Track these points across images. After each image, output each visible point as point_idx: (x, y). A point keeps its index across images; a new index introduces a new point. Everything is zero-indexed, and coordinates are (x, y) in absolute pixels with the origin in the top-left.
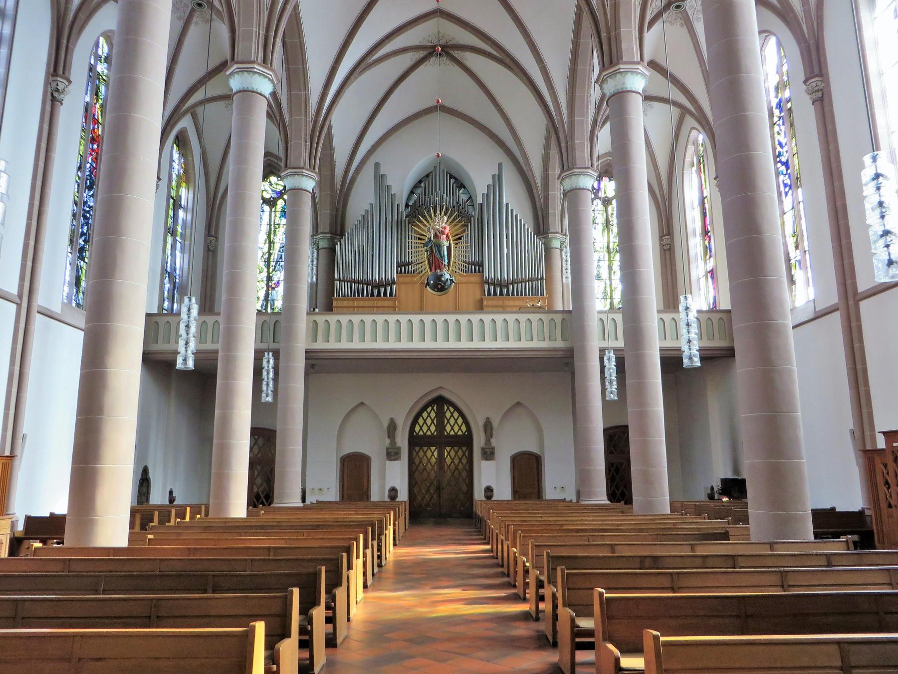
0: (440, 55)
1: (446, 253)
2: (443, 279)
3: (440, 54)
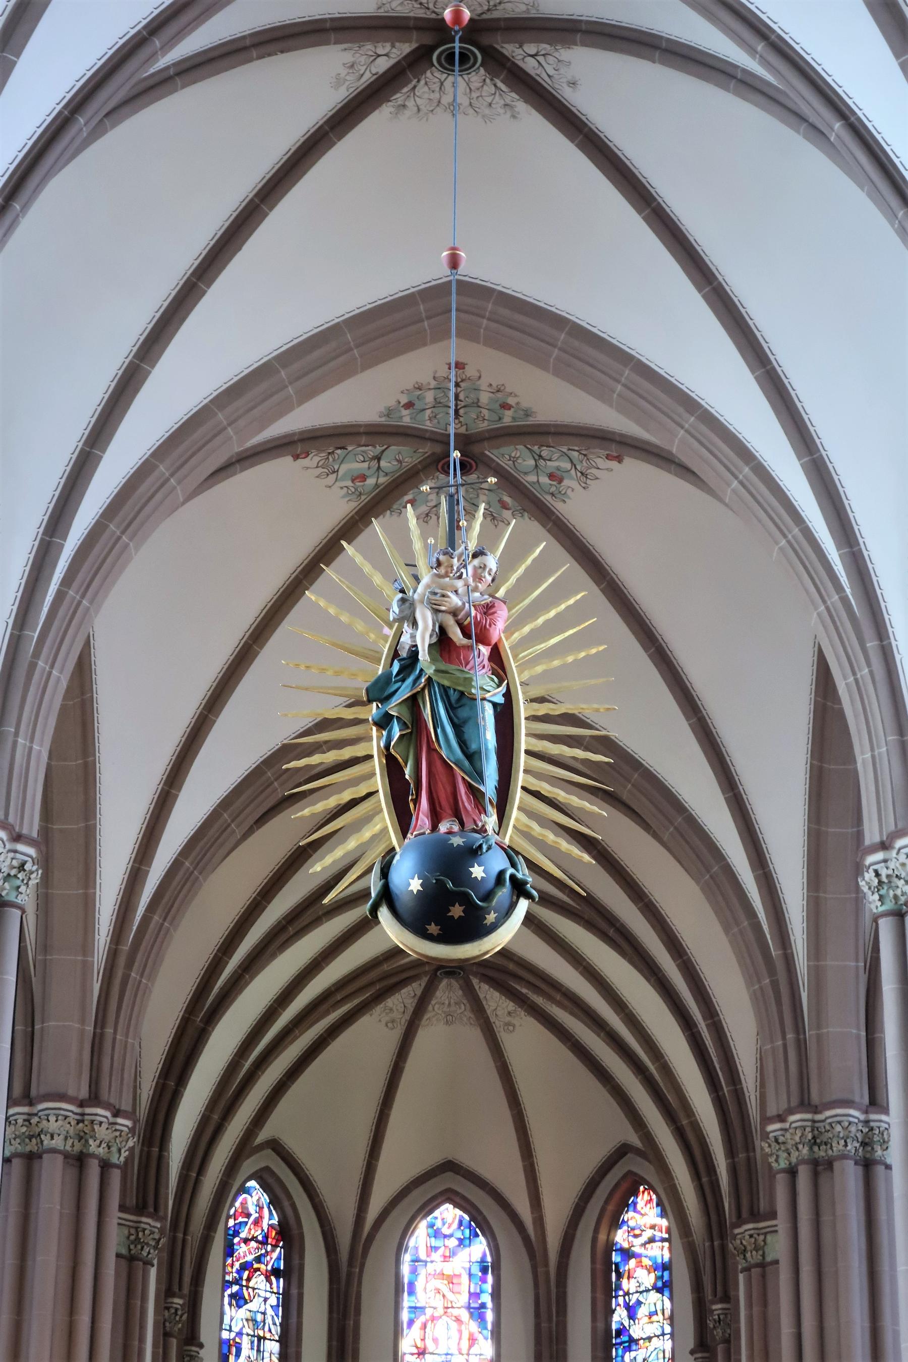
0: (464, 57)
1: (490, 737)
2: (477, 872)
3: (464, 57)
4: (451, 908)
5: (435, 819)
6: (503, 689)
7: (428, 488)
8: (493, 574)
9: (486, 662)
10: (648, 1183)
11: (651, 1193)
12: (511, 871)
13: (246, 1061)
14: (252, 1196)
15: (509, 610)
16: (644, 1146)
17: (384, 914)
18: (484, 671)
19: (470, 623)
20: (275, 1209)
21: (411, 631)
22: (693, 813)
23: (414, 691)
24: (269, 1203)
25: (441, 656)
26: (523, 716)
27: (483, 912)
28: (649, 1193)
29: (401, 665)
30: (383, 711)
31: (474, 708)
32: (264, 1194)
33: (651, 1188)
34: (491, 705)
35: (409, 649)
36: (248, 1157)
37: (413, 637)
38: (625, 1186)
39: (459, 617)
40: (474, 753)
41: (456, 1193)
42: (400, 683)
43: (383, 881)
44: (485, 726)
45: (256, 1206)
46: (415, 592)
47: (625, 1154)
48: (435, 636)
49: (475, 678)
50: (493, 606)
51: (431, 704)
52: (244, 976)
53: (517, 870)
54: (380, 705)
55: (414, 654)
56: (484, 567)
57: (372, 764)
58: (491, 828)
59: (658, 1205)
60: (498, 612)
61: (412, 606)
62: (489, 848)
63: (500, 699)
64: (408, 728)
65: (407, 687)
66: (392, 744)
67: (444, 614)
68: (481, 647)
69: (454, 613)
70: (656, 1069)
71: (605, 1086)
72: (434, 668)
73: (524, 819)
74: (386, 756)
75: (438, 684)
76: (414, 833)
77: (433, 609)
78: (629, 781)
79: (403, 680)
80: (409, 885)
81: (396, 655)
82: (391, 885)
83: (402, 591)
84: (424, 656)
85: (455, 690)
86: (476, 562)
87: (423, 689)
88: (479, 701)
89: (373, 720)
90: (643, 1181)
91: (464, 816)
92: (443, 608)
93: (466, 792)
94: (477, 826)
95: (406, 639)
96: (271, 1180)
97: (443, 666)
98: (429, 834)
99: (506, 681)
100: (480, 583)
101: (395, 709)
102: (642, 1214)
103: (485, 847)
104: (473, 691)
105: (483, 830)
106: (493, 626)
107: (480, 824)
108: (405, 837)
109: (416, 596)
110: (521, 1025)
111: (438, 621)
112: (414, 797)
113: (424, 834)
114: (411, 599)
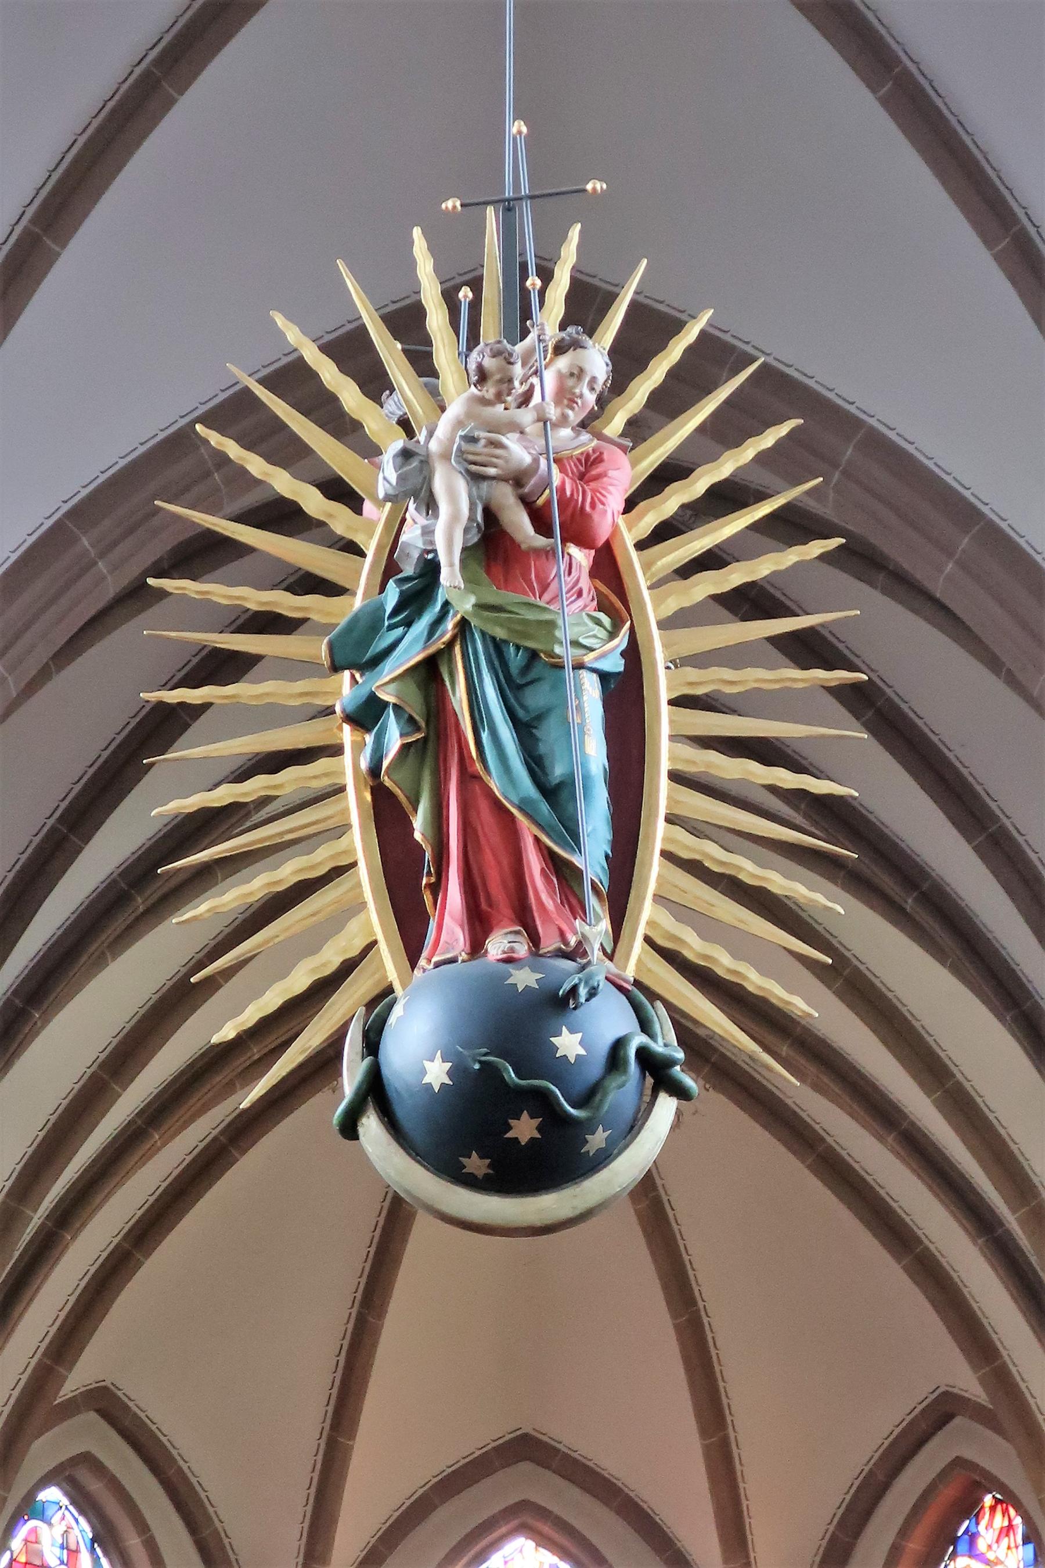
4: (513, 1122)
5: (478, 928)
6: (622, 641)
7: (458, 204)
8: (599, 387)
9: (585, 583)
10: (1002, 1488)
11: (1012, 1512)
12: (639, 1039)
13: (35, 1211)
14: (50, 1524)
15: (634, 464)
16: (992, 1401)
17: (371, 1125)
18: (580, 603)
19: (548, 503)
20: (106, 1553)
21: (425, 522)
22: (932, 1247)
23: (431, 650)
24: (93, 1541)
25: (488, 572)
26: (664, 696)
27: (578, 1130)
28: (1005, 1512)
29: (402, 593)
30: (363, 692)
31: (559, 684)
32: (81, 1519)
33: (1008, 1499)
34: (595, 677)
35: (421, 556)
36: (41, 1434)
37: (428, 532)
38: (949, 1493)
39: (526, 490)
40: (560, 785)
41: (543, 1513)
42: (399, 631)
43: (368, 1060)
44: (582, 726)
45: (62, 1547)
46: (431, 434)
47: (948, 1418)
48: (475, 531)
49: (560, 622)
50: (599, 460)
51: (465, 667)
52: (30, 1015)
53: (652, 1036)
54: (357, 676)
55: (430, 569)
56: (578, 374)
57: (342, 805)
58: (597, 946)
59: (1026, 1541)
60: (611, 473)
61: (426, 463)
62: (593, 993)
63: (615, 664)
64: (418, 729)
65: (415, 640)
66: (386, 763)
67: (494, 482)
68: (573, 550)
69: (517, 479)
70: (1021, 1222)
71: (898, 1258)
72: (473, 600)
73: (667, 921)
74: (372, 788)
75: (483, 634)
76: (435, 959)
77: (468, 471)
78: (950, 555)
79: (408, 624)
80: (424, 1072)
81: (391, 569)
82: (386, 1071)
83: (410, 432)
84: (450, 576)
85: (518, 648)
86: (563, 363)
87: (450, 645)
88: (569, 673)
89: (343, 711)
90: (991, 1483)
91: (538, 922)
92: (492, 471)
93: (543, 870)
94: (565, 942)
95: (411, 535)
96: (95, 1486)
97: (494, 595)
98: (463, 961)
99: (628, 624)
100: (573, 409)
101: (392, 687)
102: (987, 1562)
103: (583, 992)
104: (558, 650)
105: (576, 953)
106: (600, 506)
107: (573, 941)
108: (413, 963)
109: (434, 446)
110: (695, 1113)
111: (480, 498)
112: (433, 880)
113: (453, 961)
114: (422, 452)
